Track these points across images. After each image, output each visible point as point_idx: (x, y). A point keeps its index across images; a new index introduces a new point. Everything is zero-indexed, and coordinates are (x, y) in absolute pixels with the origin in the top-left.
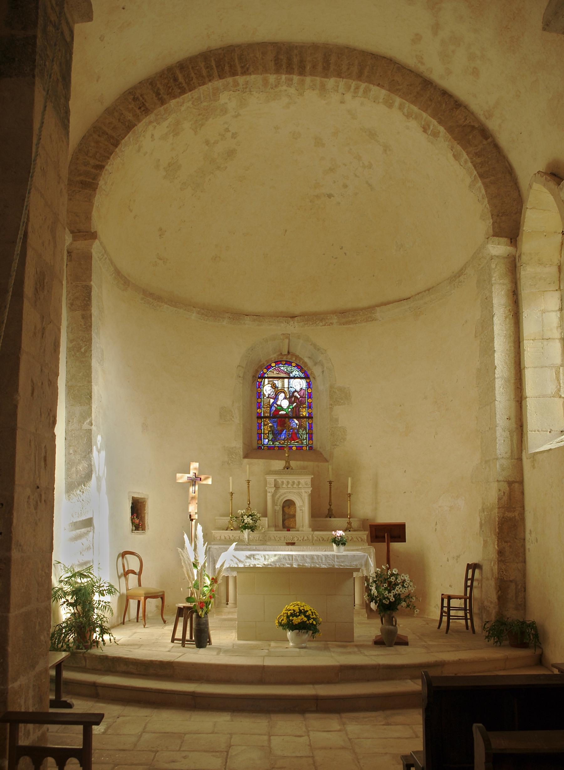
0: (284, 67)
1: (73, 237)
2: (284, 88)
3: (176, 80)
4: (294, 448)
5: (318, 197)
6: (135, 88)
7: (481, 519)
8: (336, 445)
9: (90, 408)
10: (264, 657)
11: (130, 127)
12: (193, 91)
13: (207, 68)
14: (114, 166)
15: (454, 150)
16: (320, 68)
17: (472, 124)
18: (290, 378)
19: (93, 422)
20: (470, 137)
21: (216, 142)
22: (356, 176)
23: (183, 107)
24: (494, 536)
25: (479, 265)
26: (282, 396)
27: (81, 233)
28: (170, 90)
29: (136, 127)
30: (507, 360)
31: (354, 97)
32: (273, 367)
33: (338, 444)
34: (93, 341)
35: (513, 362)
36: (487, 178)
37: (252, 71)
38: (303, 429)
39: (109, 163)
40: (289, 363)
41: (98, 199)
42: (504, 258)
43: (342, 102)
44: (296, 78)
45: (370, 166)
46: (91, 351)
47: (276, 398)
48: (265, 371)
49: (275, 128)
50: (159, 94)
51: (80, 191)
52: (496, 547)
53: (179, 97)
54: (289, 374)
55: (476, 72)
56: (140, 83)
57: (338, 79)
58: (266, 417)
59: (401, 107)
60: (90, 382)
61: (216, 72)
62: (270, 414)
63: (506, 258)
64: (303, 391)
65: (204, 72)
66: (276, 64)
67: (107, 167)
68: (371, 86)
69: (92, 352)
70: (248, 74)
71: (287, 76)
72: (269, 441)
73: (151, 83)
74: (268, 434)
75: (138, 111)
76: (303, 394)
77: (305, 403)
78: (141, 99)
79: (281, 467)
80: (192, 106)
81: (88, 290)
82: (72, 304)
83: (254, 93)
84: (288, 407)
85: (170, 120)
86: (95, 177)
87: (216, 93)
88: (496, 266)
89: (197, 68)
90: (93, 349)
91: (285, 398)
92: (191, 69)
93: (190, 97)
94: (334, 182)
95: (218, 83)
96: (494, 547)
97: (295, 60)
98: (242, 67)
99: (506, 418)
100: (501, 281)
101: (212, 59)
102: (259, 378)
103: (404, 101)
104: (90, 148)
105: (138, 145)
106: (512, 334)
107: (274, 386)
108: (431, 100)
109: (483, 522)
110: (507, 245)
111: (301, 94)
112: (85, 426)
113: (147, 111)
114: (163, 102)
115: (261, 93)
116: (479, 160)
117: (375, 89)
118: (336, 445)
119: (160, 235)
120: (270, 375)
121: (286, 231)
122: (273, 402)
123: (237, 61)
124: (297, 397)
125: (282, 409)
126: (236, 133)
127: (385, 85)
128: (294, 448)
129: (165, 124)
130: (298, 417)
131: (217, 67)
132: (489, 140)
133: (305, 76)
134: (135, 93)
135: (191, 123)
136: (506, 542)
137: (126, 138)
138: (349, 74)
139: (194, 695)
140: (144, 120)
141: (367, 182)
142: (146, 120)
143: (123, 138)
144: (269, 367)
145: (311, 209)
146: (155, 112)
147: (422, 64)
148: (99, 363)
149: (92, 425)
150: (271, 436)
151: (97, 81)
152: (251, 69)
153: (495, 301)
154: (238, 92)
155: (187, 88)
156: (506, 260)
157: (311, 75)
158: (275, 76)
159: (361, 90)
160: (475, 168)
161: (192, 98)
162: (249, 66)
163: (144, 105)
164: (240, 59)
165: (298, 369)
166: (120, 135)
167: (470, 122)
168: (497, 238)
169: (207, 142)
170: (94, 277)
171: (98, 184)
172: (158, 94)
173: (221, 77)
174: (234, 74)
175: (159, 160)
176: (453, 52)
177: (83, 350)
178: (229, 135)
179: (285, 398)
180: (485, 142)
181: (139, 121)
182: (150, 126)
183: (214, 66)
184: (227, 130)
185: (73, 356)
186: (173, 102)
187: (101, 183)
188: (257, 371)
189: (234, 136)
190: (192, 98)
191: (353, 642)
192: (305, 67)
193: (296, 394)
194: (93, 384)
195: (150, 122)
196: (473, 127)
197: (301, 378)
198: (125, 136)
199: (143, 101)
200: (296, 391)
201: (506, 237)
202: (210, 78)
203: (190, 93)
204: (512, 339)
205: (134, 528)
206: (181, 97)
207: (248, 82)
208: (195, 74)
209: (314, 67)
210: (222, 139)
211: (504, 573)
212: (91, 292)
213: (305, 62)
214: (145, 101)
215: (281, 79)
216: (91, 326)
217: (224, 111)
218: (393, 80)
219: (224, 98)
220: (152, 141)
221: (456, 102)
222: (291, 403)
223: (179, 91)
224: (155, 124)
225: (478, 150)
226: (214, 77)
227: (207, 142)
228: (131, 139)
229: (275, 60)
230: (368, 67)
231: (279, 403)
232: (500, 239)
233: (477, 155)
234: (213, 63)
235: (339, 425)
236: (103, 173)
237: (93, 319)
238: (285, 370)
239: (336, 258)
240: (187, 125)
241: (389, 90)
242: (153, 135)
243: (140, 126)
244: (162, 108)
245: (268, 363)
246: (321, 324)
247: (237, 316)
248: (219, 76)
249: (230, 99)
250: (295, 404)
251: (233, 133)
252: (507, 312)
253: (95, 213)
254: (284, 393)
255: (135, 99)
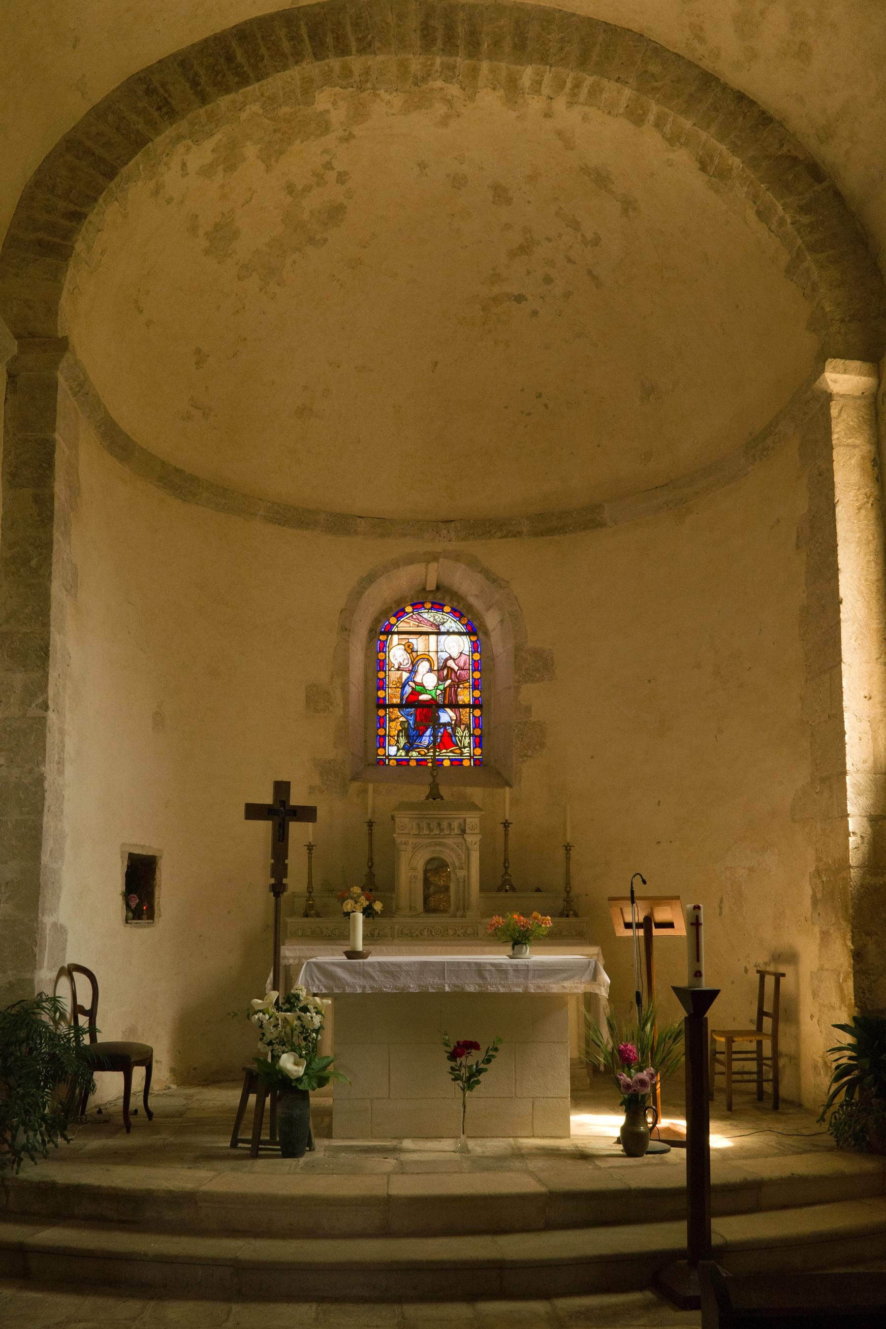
0: (439, 44)
1: (20, 346)
2: (439, 83)
3: (230, 58)
4: (447, 763)
5: (497, 300)
6: (149, 70)
7: (813, 890)
8: (526, 755)
9: (46, 676)
10: (388, 1175)
11: (139, 143)
12: (264, 82)
13: (292, 39)
14: (106, 215)
15: (758, 203)
16: (507, 45)
17: (794, 153)
18: (439, 633)
19: (50, 703)
20: (790, 178)
21: (307, 189)
22: (569, 260)
23: (246, 109)
24: (844, 924)
25: (805, 414)
26: (424, 666)
27: (36, 340)
28: (219, 78)
29: (150, 144)
30: (862, 588)
31: (570, 104)
32: (408, 614)
33: (530, 753)
34: (56, 547)
35: (874, 589)
36: (822, 252)
37: (379, 49)
38: (463, 727)
39: (95, 211)
40: (438, 606)
41: (75, 276)
42: (855, 398)
43: (548, 115)
44: (461, 62)
45: (596, 241)
46: (51, 565)
47: (413, 671)
48: (393, 620)
49: (419, 165)
50: (198, 84)
51: (36, 260)
52: (849, 944)
53: (236, 91)
54: (438, 626)
55: (803, 52)
56: (160, 61)
57: (542, 67)
58: (393, 706)
59: (659, 124)
60: (46, 625)
61: (309, 46)
62: (402, 699)
63: (859, 398)
64: (463, 658)
65: (286, 46)
66: (424, 37)
67: (91, 217)
68: (605, 82)
69: (53, 567)
70: (371, 53)
71: (444, 58)
72: (398, 750)
73: (182, 61)
74: (398, 736)
75: (156, 114)
76: (465, 664)
77: (467, 681)
78: (161, 91)
79: (422, 797)
80: (261, 112)
81: (47, 451)
82: (14, 475)
83: (382, 92)
84: (436, 688)
85: (218, 137)
86: (68, 235)
87: (308, 88)
88: (840, 413)
89: (273, 38)
90: (54, 560)
91: (431, 670)
92: (259, 40)
93: (258, 94)
94: (529, 273)
95: (310, 68)
96: (845, 945)
97: (461, 30)
98: (359, 40)
99: (863, 693)
100: (850, 441)
101: (302, 23)
102: (382, 633)
103: (667, 110)
104: (58, 180)
105: (154, 181)
106: (871, 538)
107: (410, 649)
108: (716, 110)
109: (819, 896)
110: (861, 374)
111: (472, 98)
112: (33, 711)
113: (171, 114)
114: (204, 99)
115: (395, 94)
116: (805, 219)
117: (610, 87)
118: (526, 755)
119: (197, 363)
120: (401, 629)
121: (436, 363)
122: (408, 678)
123: (349, 28)
124: (452, 669)
125: (425, 691)
126: (346, 173)
127: (631, 81)
128: (447, 763)
129: (209, 144)
130: (455, 706)
131: (310, 37)
132: (826, 184)
133: (479, 60)
134: (150, 79)
135: (259, 146)
136: (868, 934)
137: (132, 163)
138: (562, 59)
139: (237, 1266)
140: (167, 132)
141: (590, 273)
142: (170, 132)
143: (126, 164)
144: (400, 614)
145: (484, 324)
146: (190, 116)
147: (702, 41)
148: (67, 590)
149: (46, 708)
150: (403, 741)
151: (74, 48)
152: (377, 44)
153: (839, 478)
154: (350, 89)
155: (252, 75)
156: (859, 401)
157: (490, 58)
158: (422, 59)
159: (584, 91)
160: (799, 233)
161: (262, 95)
162: (373, 37)
163: (167, 103)
164: (356, 25)
165: (455, 616)
166: (118, 158)
167: (789, 151)
168: (843, 361)
169: (290, 188)
170: (60, 423)
171: (73, 248)
172: (195, 84)
173: (318, 55)
174: (343, 51)
175: (197, 216)
176: (762, 13)
177: (33, 563)
178: (332, 176)
179: (431, 670)
180: (817, 187)
181: (158, 132)
182: (178, 146)
183: (306, 37)
184: (328, 166)
185: (13, 574)
186: (224, 102)
187: (79, 246)
188: (377, 621)
189: (342, 178)
190: (262, 95)
191: (568, 1136)
192: (479, 44)
193: (451, 663)
194: (52, 629)
195: (180, 138)
196: (795, 159)
197: (460, 634)
198: (130, 159)
199: (166, 95)
200: (451, 658)
201: (858, 359)
202: (298, 57)
203: (257, 85)
204: (872, 547)
205: (130, 915)
206: (241, 91)
207: (369, 68)
208: (268, 49)
209: (497, 43)
210: (318, 184)
211: (868, 995)
212: (53, 452)
213: (480, 33)
214: (170, 96)
215: (432, 64)
216: (51, 518)
217: (325, 127)
218: (646, 72)
219: (322, 101)
220: (183, 176)
221: (764, 112)
222: (441, 679)
223: (236, 79)
224: (189, 142)
225: (804, 202)
226: (304, 56)
227: (290, 188)
228: (141, 167)
229: (423, 29)
230: (598, 46)
231: (418, 679)
232: (848, 362)
233: (804, 209)
234: (304, 31)
235: (533, 719)
236: (84, 229)
237: (56, 504)
238: (432, 620)
239: (529, 414)
240: (251, 150)
241: (638, 90)
242: (184, 165)
243: (159, 142)
244: (202, 111)
245: (398, 605)
246: (499, 534)
247: (340, 524)
248: (315, 54)
249: (334, 103)
250: (449, 682)
251: (339, 173)
252: (861, 497)
253: (64, 302)
254: (428, 660)
255: (150, 91)
